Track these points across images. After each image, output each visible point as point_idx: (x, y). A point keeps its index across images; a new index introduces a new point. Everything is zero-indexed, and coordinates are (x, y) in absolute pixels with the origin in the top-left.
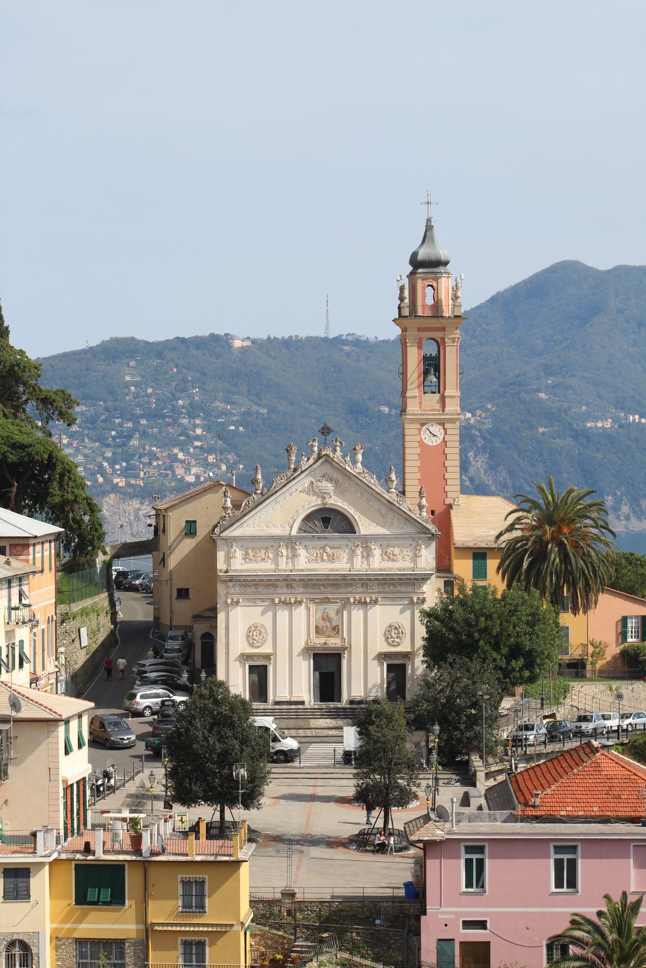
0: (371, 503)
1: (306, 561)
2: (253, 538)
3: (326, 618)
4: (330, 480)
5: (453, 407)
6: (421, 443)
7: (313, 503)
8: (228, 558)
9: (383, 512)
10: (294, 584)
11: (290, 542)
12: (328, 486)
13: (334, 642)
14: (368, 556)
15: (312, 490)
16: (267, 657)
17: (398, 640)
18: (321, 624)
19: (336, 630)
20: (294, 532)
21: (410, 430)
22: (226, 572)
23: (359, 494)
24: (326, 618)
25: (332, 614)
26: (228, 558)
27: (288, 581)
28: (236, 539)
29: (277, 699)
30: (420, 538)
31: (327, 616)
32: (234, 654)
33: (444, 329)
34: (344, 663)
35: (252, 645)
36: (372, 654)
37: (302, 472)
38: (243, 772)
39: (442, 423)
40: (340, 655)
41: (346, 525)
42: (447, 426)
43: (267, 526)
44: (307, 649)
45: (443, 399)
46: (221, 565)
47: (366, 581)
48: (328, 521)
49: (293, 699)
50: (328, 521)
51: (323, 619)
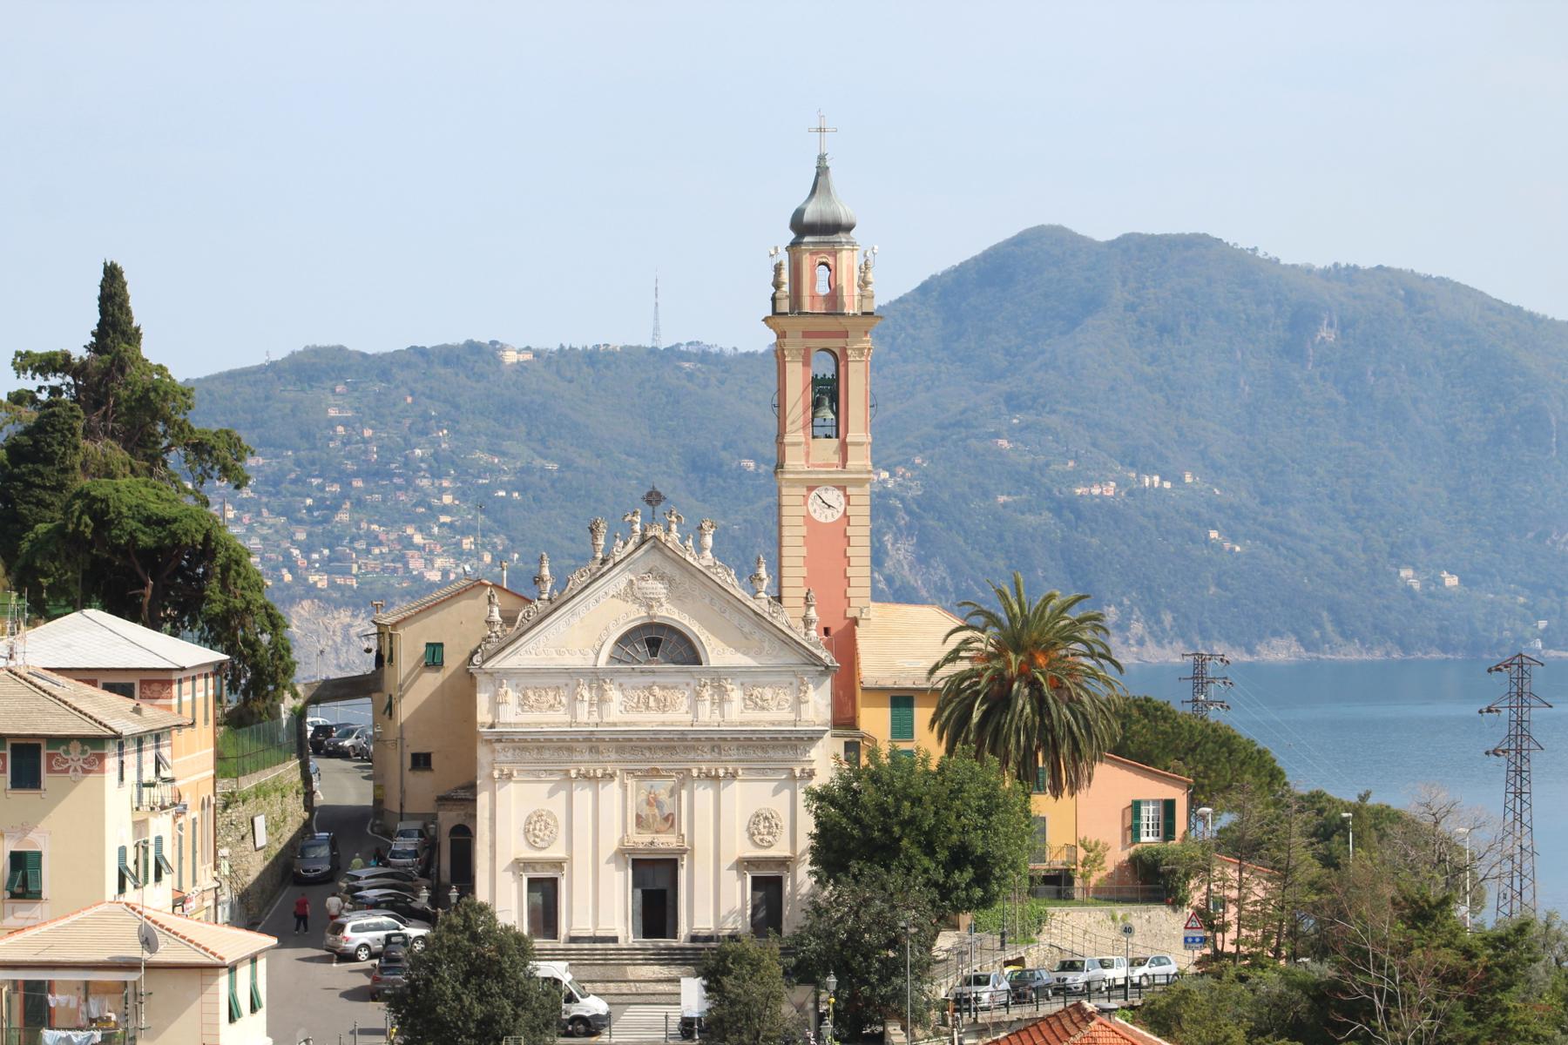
0: (727, 615)
1: (621, 710)
3: (653, 802)
4: (662, 577)
5: (860, 460)
6: (808, 518)
7: (634, 615)
9: (746, 630)
10: (602, 746)
12: (657, 588)
13: (666, 841)
14: (722, 701)
16: (558, 864)
17: (770, 838)
19: (670, 821)
20: (602, 662)
21: (791, 498)
22: (492, 726)
23: (707, 601)
24: (653, 802)
25: (663, 796)
26: (495, 704)
27: (593, 742)
28: (508, 673)
29: (574, 933)
30: (805, 673)
31: (655, 799)
32: (504, 860)
33: (845, 334)
35: (532, 845)
37: (615, 565)
39: (842, 487)
40: (675, 861)
41: (685, 651)
42: (849, 491)
43: (559, 653)
44: (622, 852)
45: (844, 447)
47: (718, 742)
48: (657, 643)
49: (598, 934)
50: (657, 643)
51: (649, 803)
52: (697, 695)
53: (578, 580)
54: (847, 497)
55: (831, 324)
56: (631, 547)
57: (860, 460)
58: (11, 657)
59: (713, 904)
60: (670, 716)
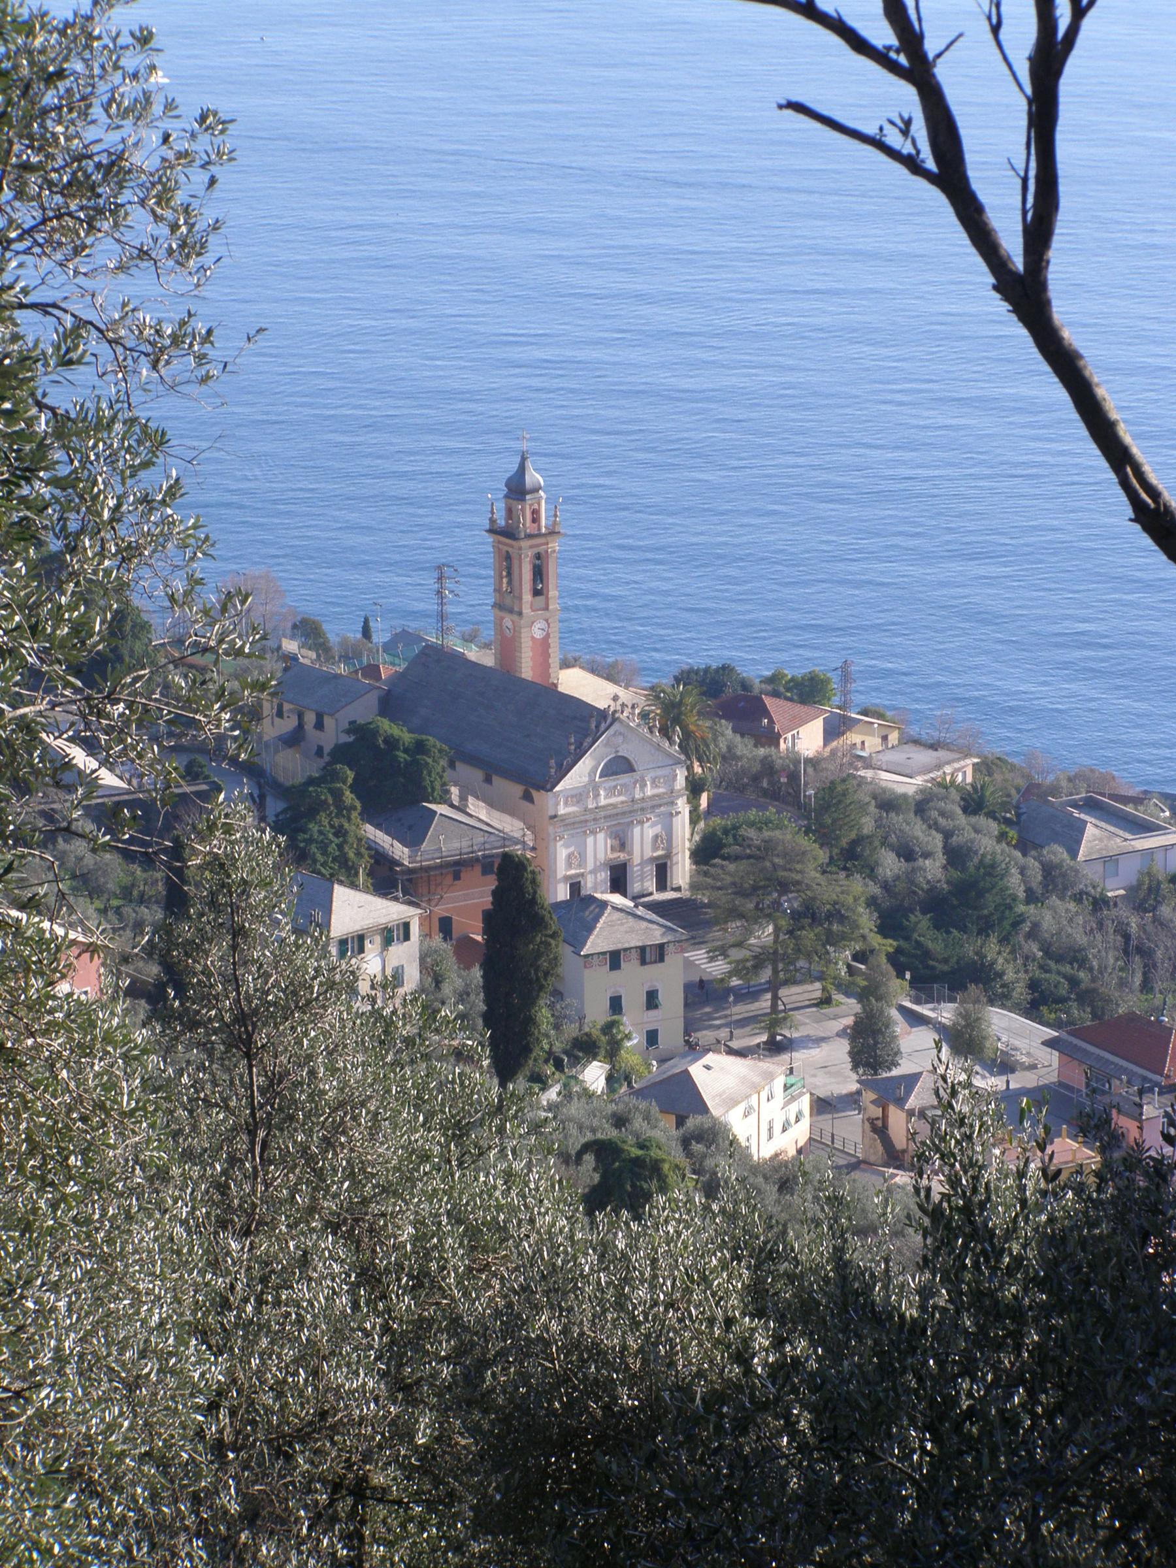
13: (622, 856)
45: (547, 599)
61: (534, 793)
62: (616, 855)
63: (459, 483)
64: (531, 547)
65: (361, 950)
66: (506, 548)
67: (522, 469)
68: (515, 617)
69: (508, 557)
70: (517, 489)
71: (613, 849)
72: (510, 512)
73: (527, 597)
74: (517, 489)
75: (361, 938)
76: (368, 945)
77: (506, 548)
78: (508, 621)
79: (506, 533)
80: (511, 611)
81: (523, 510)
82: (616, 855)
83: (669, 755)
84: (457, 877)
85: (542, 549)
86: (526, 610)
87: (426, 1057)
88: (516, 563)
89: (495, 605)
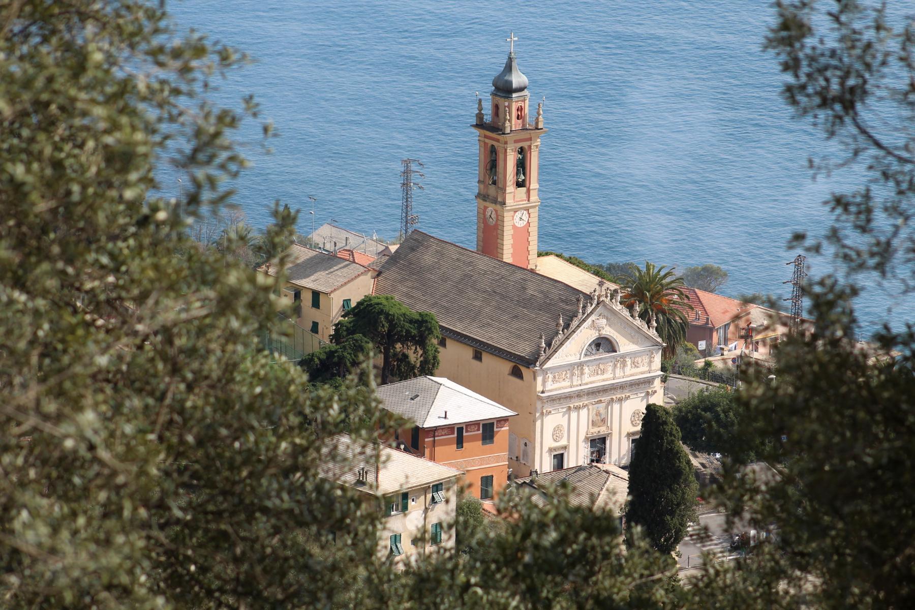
1: (591, 379)
2: (560, 367)
4: (604, 317)
5: (534, 197)
6: (514, 226)
7: (593, 335)
8: (544, 382)
11: (581, 365)
12: (603, 322)
13: (603, 430)
14: (624, 366)
15: (593, 326)
16: (565, 448)
18: (595, 418)
21: (507, 216)
22: (543, 392)
24: (598, 414)
25: (602, 411)
26: (544, 382)
28: (549, 369)
32: (545, 449)
33: (530, 139)
34: (608, 442)
35: (555, 441)
36: (624, 434)
38: (856, 591)
39: (527, 209)
42: (531, 211)
44: (587, 438)
45: (528, 191)
46: (539, 388)
47: (622, 387)
48: (603, 344)
50: (603, 344)
52: (615, 366)
53: (575, 323)
54: (529, 214)
55: (525, 135)
56: (594, 306)
57: (534, 197)
58: (445, 417)
59: (353, 378)
60: (605, 376)
61: (523, 369)
62: (596, 430)
63: (286, 96)
64: (516, 141)
65: (405, 508)
66: (490, 142)
67: (509, 68)
68: (498, 207)
69: (493, 151)
70: (504, 90)
71: (594, 424)
72: (496, 107)
73: (510, 188)
74: (504, 90)
75: (405, 496)
76: (411, 504)
77: (490, 142)
78: (491, 208)
79: (490, 126)
80: (495, 201)
81: (509, 107)
82: (596, 430)
83: (648, 338)
84: (460, 442)
85: (525, 144)
86: (509, 201)
87: (210, 593)
88: (501, 156)
89: (478, 196)
